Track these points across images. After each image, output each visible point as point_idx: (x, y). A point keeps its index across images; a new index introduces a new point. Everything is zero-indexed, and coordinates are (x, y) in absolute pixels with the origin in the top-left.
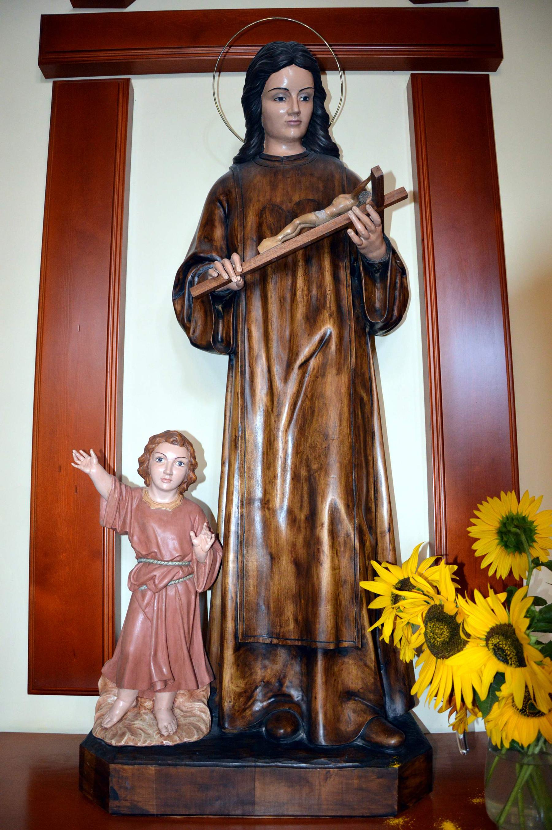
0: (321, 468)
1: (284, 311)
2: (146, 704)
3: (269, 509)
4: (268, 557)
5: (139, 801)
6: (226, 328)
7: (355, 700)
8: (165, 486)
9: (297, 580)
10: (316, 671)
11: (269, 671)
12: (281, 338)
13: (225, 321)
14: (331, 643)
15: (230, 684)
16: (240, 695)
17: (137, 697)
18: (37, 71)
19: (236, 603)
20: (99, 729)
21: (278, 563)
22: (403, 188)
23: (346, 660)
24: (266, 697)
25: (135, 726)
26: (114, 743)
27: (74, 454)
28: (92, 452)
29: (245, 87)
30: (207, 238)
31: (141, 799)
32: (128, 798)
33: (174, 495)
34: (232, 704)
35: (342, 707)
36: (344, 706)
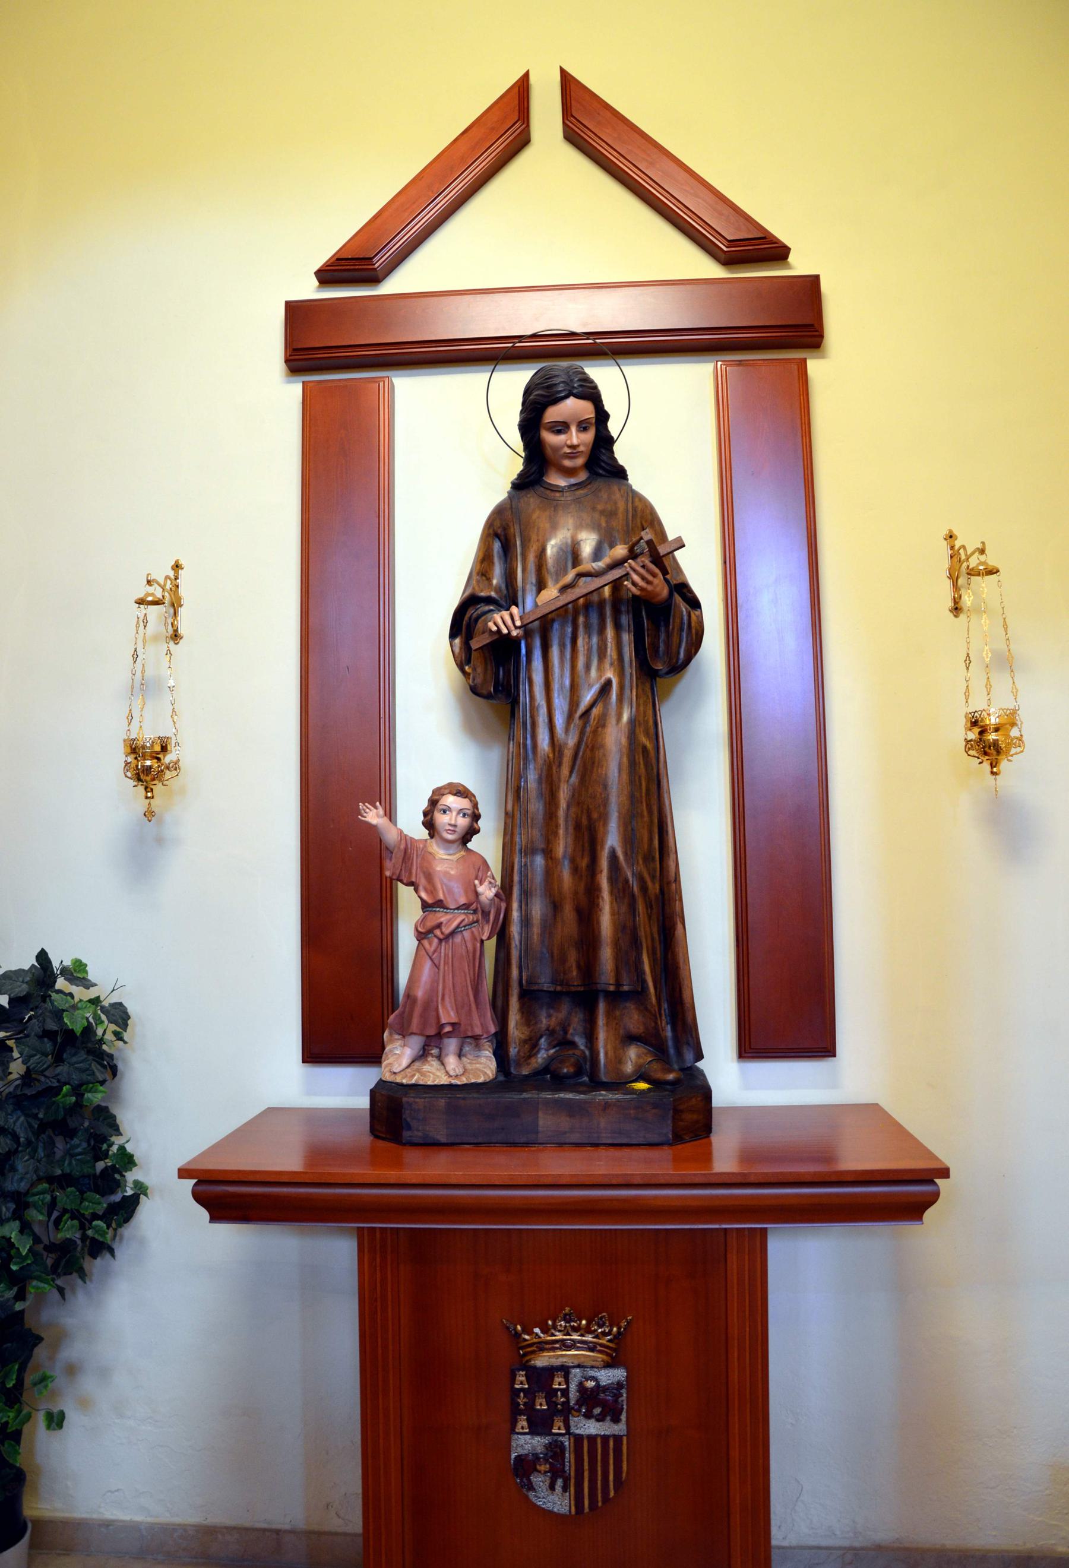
3: (551, 858)
6: (507, 673)
7: (637, 1045)
8: (450, 837)
11: (554, 1019)
14: (612, 984)
15: (515, 1030)
16: (525, 1041)
19: (521, 951)
22: (680, 537)
23: (628, 1004)
24: (551, 1046)
26: (404, 1081)
27: (361, 807)
29: (522, 412)
32: (420, 1128)
33: (458, 846)
35: (624, 1050)
36: (626, 1050)
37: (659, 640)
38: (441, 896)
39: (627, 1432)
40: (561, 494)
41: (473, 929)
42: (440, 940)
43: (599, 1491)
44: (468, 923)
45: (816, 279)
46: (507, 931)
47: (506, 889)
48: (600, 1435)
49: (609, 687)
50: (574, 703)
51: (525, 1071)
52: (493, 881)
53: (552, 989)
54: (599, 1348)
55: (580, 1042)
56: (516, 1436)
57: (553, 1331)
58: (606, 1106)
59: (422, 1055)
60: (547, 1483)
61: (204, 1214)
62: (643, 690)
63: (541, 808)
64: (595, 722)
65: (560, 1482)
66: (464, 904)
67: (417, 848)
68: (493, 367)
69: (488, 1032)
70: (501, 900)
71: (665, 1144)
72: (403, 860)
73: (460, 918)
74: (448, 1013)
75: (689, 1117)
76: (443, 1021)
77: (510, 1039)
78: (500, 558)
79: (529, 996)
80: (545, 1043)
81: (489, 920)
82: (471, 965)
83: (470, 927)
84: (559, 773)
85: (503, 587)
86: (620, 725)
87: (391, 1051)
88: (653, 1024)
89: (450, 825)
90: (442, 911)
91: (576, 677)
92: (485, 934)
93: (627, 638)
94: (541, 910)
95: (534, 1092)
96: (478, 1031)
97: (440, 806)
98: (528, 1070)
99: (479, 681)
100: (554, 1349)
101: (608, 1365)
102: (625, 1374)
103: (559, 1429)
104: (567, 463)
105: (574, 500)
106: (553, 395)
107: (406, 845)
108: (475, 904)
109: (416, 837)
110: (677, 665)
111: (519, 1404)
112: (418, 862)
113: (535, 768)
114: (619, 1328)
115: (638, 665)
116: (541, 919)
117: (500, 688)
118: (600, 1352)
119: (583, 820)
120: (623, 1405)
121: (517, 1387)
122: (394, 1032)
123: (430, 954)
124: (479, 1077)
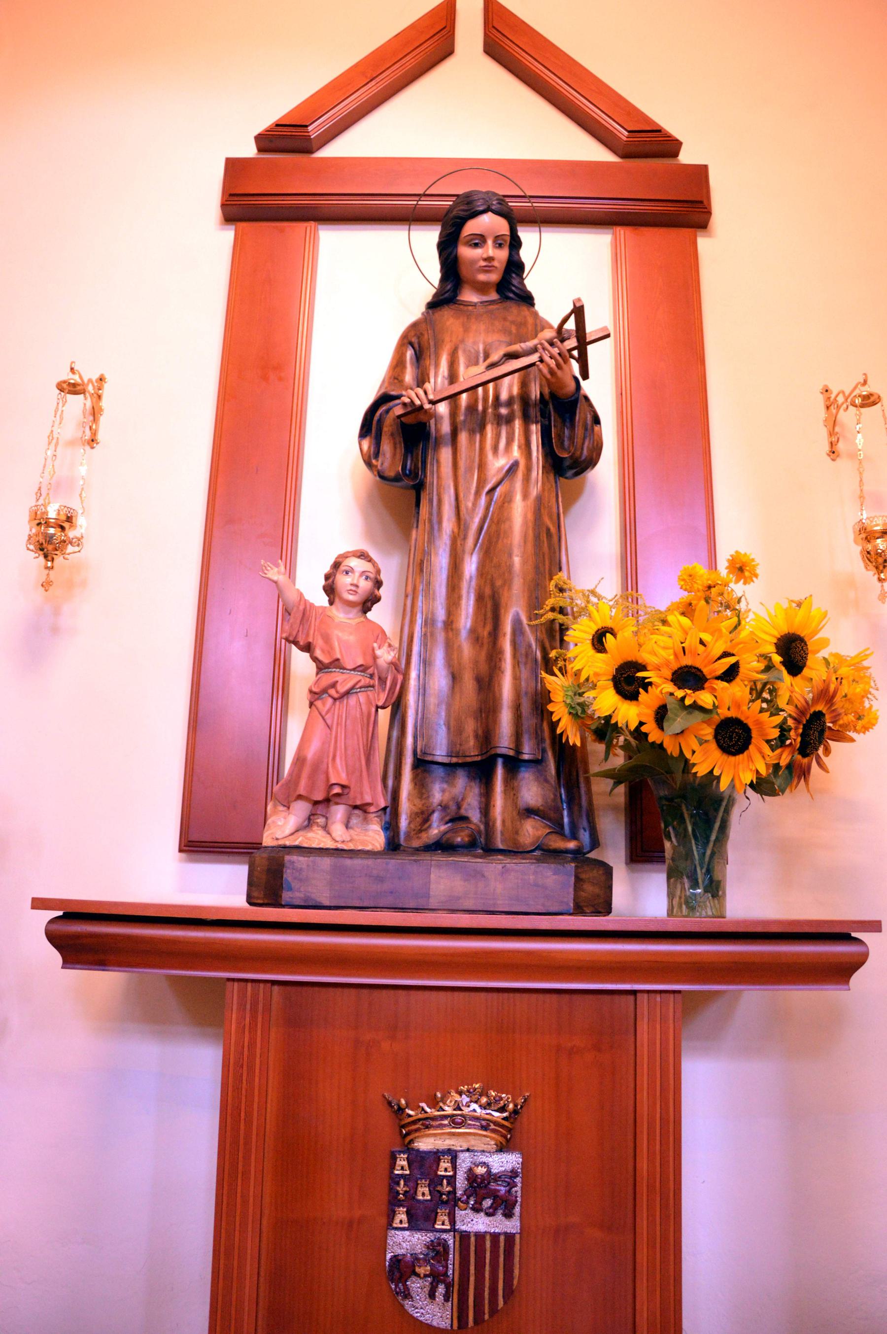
0: (504, 584)
2: (318, 821)
4: (450, 677)
8: (351, 598)
9: (479, 694)
11: (447, 794)
17: (310, 816)
30: (397, 379)
31: (315, 891)
38: (339, 656)
39: (521, 1229)
43: (487, 1302)
45: (704, 169)
48: (490, 1234)
54: (492, 1127)
56: (393, 1232)
57: (441, 1104)
59: (309, 823)
60: (427, 1290)
61: (55, 957)
65: (441, 1289)
72: (301, 622)
78: (412, 364)
79: (422, 764)
81: (385, 687)
82: (365, 729)
83: (366, 689)
84: (463, 545)
89: (352, 585)
93: (535, 428)
97: (342, 568)
100: (442, 1126)
101: (501, 1149)
102: (521, 1160)
103: (443, 1224)
104: (482, 277)
108: (372, 668)
109: (317, 604)
111: (398, 1193)
114: (516, 1105)
118: (494, 1131)
120: (516, 1197)
121: (397, 1172)
122: (278, 804)
123: (323, 714)
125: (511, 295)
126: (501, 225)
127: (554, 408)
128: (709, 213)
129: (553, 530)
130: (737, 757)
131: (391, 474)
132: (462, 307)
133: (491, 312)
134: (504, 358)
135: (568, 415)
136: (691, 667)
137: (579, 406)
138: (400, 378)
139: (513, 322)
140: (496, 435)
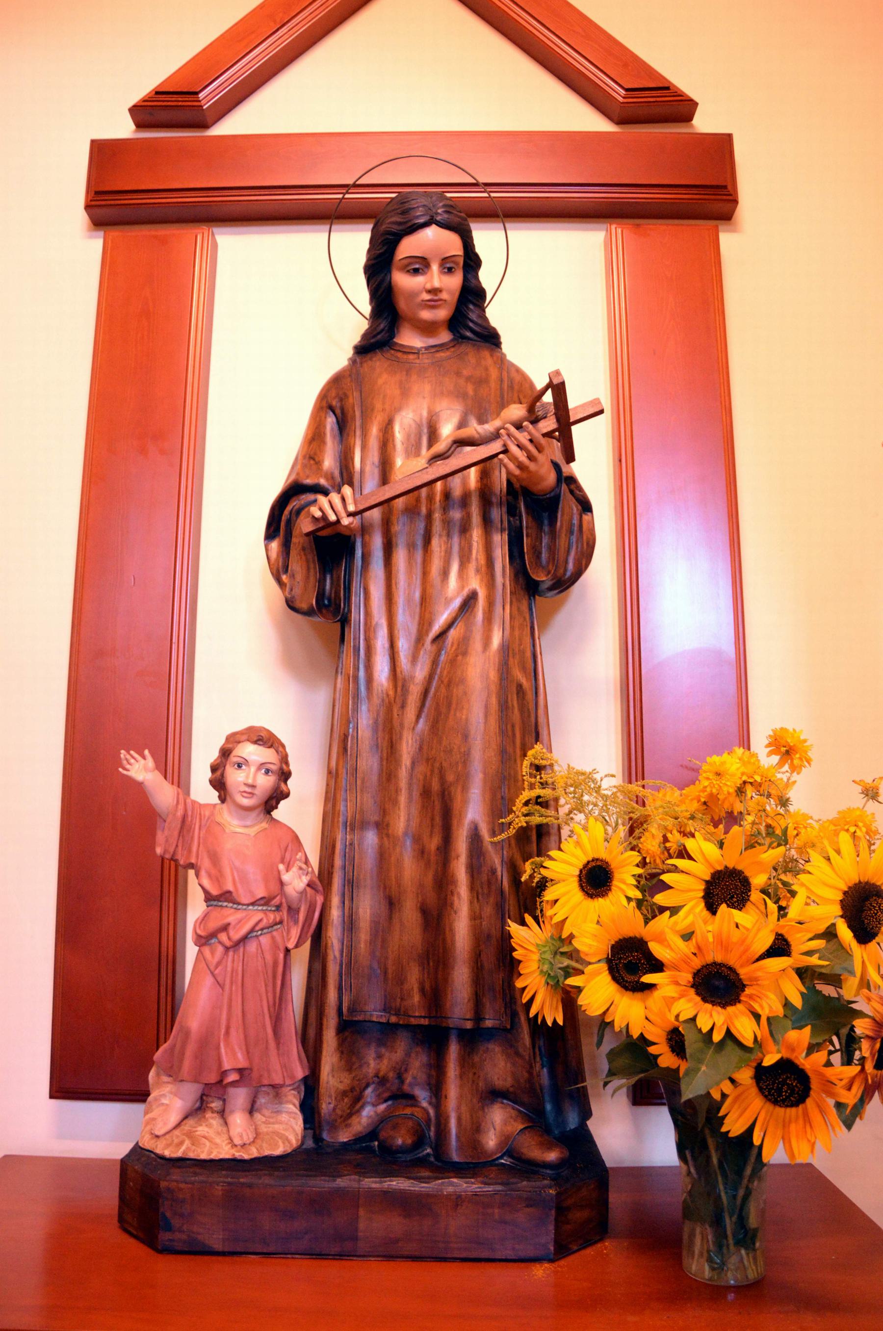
1: (414, 564)
2: (213, 1105)
3: (388, 835)
5: (199, 1234)
6: (335, 584)
7: (502, 1103)
8: (246, 802)
9: (424, 933)
10: (447, 1061)
11: (385, 1061)
12: (409, 600)
13: (334, 576)
14: (468, 1020)
16: (344, 1094)
17: (203, 1095)
18: (80, 217)
19: (341, 965)
20: (147, 1137)
21: (400, 910)
23: (491, 1046)
25: (197, 1133)
26: (167, 1153)
27: (122, 756)
28: (146, 752)
29: (369, 251)
30: (314, 459)
31: (201, 1230)
32: (185, 1228)
33: (258, 815)
34: (332, 1106)
35: (484, 1112)
36: (486, 1110)
37: (541, 544)
38: (230, 887)
40: (416, 356)
41: (275, 933)
42: (227, 949)
44: (268, 925)
46: (323, 935)
47: (325, 877)
49: (472, 601)
50: (425, 623)
51: (344, 1137)
52: (304, 866)
53: (384, 1020)
55: (423, 1096)
58: (457, 1200)
59: (198, 1109)
62: (519, 609)
63: (376, 764)
64: (454, 648)
66: (261, 898)
67: (200, 814)
68: (340, 207)
69: (292, 1077)
70: (316, 891)
71: (544, 1260)
73: (256, 916)
74: (234, 1054)
75: (578, 1216)
76: (227, 1066)
77: (322, 1090)
78: (334, 437)
80: (373, 1095)
83: (270, 930)
84: (401, 716)
85: (337, 473)
86: (488, 653)
87: (156, 1099)
88: (526, 1075)
89: (246, 785)
90: (231, 907)
91: (428, 587)
92: (292, 940)
94: (370, 909)
95: (353, 1177)
96: (277, 1079)
97: (233, 759)
98: (347, 1134)
99: (297, 591)
104: (426, 315)
105: (433, 363)
106: (410, 221)
107: (186, 810)
108: (278, 898)
110: (563, 579)
112: (201, 835)
113: (369, 710)
115: (512, 575)
116: (371, 921)
117: (326, 602)
119: (433, 784)
122: (162, 1072)
123: (212, 968)
124: (276, 1146)
125: (468, 334)
126: (451, 243)
127: (527, 507)
128: (734, 202)
129: (526, 684)
130: (788, 1110)
131: (304, 606)
132: (399, 355)
133: (438, 364)
134: (455, 446)
135: (546, 515)
136: (721, 965)
137: (560, 506)
138: (317, 459)
139: (468, 379)
140: (446, 552)
